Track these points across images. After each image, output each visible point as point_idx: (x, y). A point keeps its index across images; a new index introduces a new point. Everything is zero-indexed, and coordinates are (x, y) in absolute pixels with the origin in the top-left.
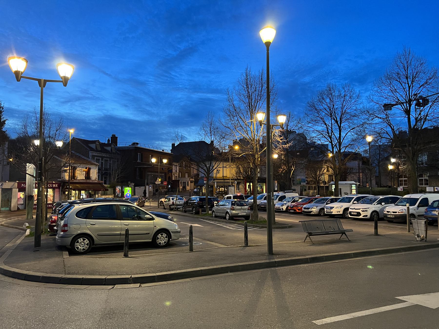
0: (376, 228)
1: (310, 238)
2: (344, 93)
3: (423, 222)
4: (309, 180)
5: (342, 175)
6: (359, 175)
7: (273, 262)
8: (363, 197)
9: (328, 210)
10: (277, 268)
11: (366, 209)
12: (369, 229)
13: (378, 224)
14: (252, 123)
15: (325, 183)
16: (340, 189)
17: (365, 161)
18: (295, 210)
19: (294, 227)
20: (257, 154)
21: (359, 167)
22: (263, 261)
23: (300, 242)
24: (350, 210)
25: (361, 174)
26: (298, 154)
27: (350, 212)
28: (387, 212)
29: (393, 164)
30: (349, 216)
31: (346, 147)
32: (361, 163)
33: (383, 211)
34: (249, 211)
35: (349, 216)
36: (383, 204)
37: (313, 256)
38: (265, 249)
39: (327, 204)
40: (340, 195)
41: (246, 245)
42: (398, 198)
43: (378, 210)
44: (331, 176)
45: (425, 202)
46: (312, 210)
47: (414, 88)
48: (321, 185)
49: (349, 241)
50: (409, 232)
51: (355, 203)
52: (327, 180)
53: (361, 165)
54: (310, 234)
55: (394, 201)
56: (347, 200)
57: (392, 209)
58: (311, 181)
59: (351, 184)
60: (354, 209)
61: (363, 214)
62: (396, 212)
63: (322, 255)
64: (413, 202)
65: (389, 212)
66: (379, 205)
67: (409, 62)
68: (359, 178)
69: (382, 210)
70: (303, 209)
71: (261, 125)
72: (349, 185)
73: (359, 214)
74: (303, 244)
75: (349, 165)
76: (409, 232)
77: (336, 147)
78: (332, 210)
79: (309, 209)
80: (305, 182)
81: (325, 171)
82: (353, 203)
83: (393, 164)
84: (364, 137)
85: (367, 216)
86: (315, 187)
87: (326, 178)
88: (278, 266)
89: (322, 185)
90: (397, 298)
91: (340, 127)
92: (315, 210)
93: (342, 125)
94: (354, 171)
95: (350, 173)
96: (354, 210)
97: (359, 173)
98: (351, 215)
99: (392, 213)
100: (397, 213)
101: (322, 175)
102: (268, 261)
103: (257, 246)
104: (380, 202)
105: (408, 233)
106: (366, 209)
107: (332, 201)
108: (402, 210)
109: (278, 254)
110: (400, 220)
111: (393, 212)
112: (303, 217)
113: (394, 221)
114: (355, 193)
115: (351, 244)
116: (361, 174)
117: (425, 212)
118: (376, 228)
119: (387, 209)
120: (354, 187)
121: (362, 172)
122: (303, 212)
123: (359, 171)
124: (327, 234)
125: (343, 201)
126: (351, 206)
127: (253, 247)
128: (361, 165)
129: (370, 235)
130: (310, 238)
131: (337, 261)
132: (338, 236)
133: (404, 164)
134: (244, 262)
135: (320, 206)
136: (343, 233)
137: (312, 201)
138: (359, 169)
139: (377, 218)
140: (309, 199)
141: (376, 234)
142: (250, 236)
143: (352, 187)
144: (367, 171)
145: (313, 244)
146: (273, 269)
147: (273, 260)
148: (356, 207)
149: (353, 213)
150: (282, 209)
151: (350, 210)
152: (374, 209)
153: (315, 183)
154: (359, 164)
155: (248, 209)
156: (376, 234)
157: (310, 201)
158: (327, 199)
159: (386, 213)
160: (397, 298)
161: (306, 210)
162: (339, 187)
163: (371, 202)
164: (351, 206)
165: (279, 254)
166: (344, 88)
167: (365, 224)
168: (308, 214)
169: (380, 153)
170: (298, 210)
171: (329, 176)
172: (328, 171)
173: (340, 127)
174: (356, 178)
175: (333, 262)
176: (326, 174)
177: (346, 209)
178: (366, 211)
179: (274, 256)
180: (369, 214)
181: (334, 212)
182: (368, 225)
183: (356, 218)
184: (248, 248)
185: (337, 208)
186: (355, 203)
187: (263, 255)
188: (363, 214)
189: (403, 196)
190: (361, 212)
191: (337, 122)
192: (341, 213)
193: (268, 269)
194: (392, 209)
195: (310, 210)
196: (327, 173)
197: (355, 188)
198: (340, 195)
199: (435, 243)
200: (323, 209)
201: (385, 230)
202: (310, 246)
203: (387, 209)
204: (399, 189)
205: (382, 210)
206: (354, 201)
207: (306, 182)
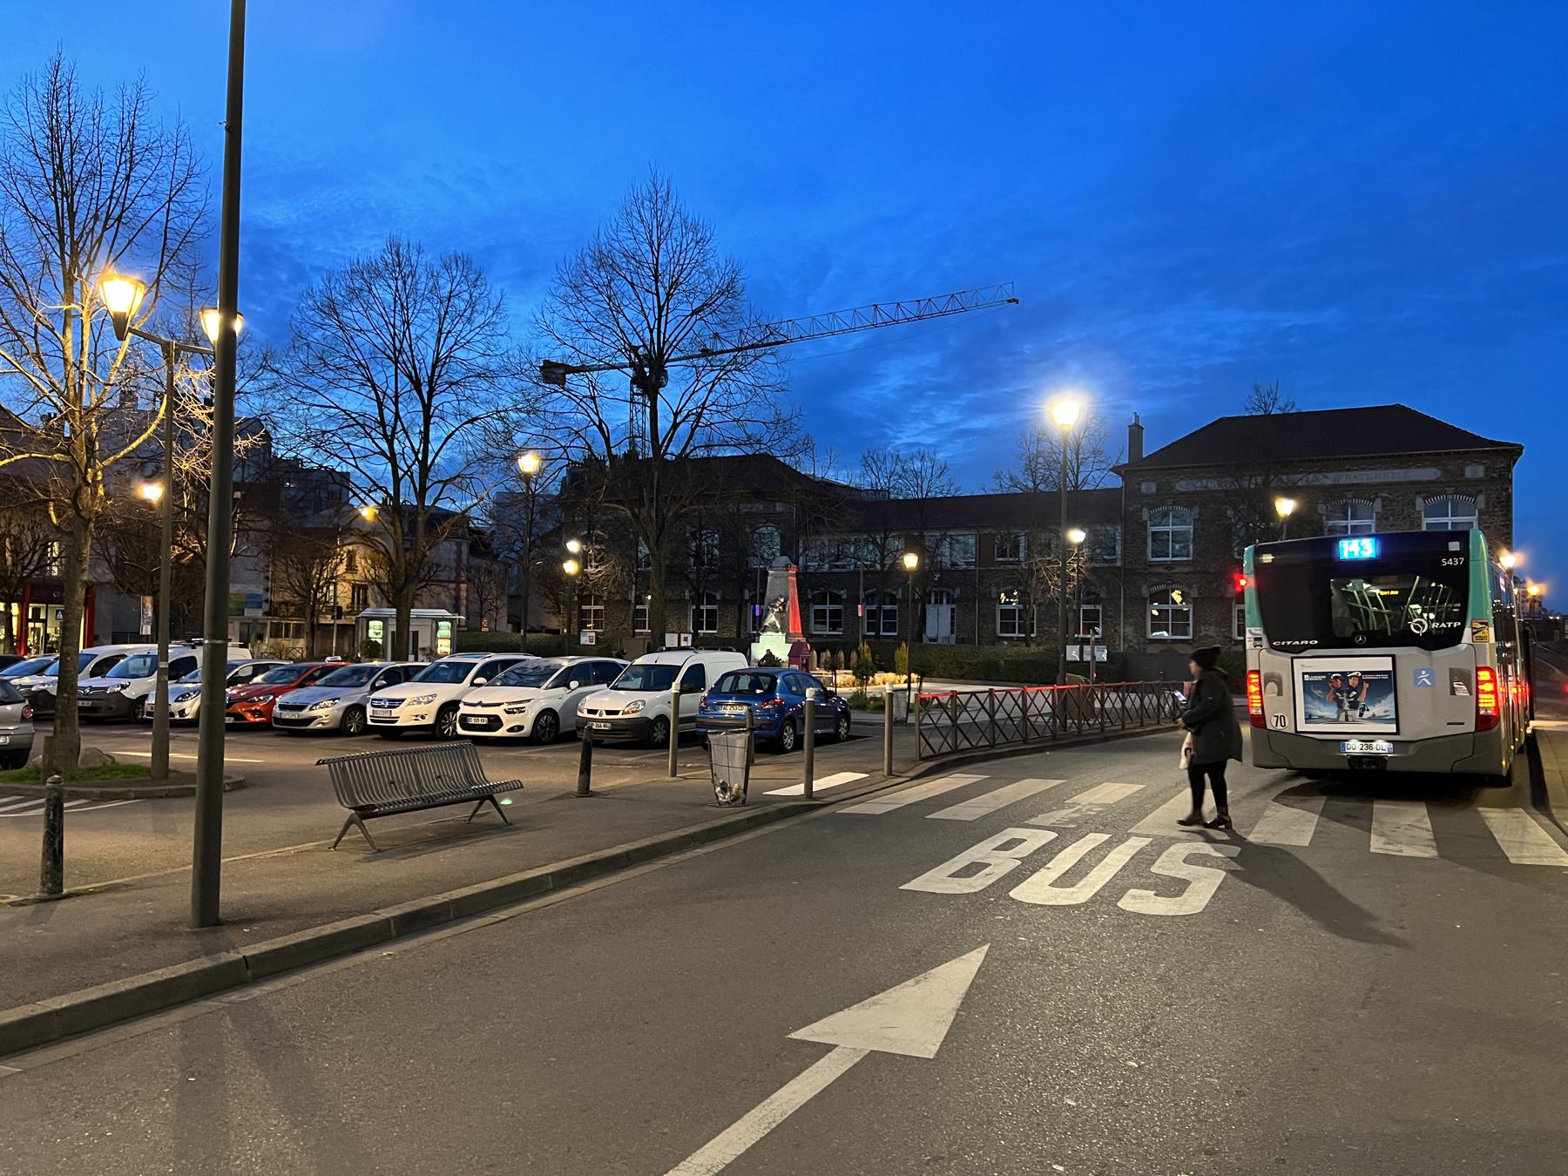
0: (585, 769)
1: (362, 826)
2: (448, 288)
3: (740, 741)
4: (277, 598)
5: (401, 587)
6: (458, 590)
7: (224, 959)
8: (506, 664)
9: (381, 713)
10: (256, 992)
11: (515, 705)
12: (554, 773)
13: (594, 757)
14: (72, 321)
15: (338, 612)
16: (416, 634)
17: (479, 543)
18: (238, 716)
19: (253, 785)
20: (93, 467)
21: (459, 560)
22: (181, 969)
23: (316, 850)
24: (463, 710)
25: (463, 586)
26: (238, 495)
27: (464, 717)
28: (590, 711)
29: (569, 556)
30: (460, 731)
31: (445, 483)
32: (465, 549)
33: (576, 708)
34: (29, 727)
35: (460, 731)
36: (574, 684)
37: (407, 908)
38: (182, 897)
39: (374, 689)
40: (411, 657)
41: (51, 892)
42: (618, 668)
43: (557, 705)
44: (360, 587)
45: (696, 677)
46: (315, 713)
47: (670, 317)
48: (322, 621)
49: (506, 826)
50: (674, 775)
51: (480, 685)
52: (344, 602)
53: (464, 557)
54: (365, 812)
55: (605, 675)
56: (449, 675)
57: (607, 703)
58: (286, 603)
59: (437, 620)
60: (480, 704)
61: (508, 722)
62: (617, 712)
63: (440, 899)
64: (659, 678)
65: (594, 712)
66: (562, 690)
67: (666, 224)
68: (457, 598)
69: (574, 704)
70: (276, 710)
71: (121, 337)
72: (429, 622)
73: (495, 722)
74: (333, 856)
75: (421, 549)
76: (674, 775)
77: (411, 477)
78: (395, 712)
79: (301, 708)
80: (260, 607)
81: (342, 568)
82: (472, 684)
83: (574, 557)
84: (512, 458)
85: (521, 728)
86: (298, 628)
87: (343, 594)
88: (257, 979)
89: (327, 620)
90: (794, 1036)
91: (427, 408)
92: (326, 712)
93: (435, 403)
94: (443, 575)
95: (429, 581)
96: (479, 710)
97: (458, 582)
98: (465, 726)
99: (605, 716)
100: (620, 716)
101: (328, 583)
102: (205, 963)
103: (108, 889)
104: (563, 681)
105: (668, 778)
106: (515, 705)
107: (393, 677)
108: (635, 703)
109: (242, 920)
110: (639, 737)
111: (608, 713)
112: (278, 741)
113: (606, 741)
114: (448, 650)
115: (522, 836)
116: (463, 586)
117: (702, 709)
118: (585, 769)
119: (589, 702)
120: (445, 629)
121: (469, 580)
122: (278, 720)
123: (458, 575)
124: (431, 804)
125: (433, 676)
126: (465, 693)
127: (92, 899)
128: (464, 557)
129: (562, 797)
130: (362, 826)
131: (503, 915)
132: (459, 813)
133: (601, 561)
134: (77, 987)
135: (346, 698)
136: (487, 796)
137: (312, 679)
138: (458, 568)
139: (551, 731)
140: (299, 671)
141: (585, 790)
142: (75, 844)
143: (437, 628)
144: (491, 573)
145: (377, 851)
146: (235, 997)
147: (234, 956)
148: (484, 699)
149: (472, 721)
150: (182, 712)
151: (463, 710)
152: (544, 704)
153: (300, 612)
154: (459, 553)
155: (23, 719)
156: (585, 790)
157: (306, 680)
158: (374, 670)
159: (585, 715)
160: (794, 1036)
161: (287, 715)
162: (412, 629)
163: (534, 679)
164: (465, 693)
165: (248, 921)
166: (447, 268)
167: (516, 758)
168: (299, 731)
169: (536, 518)
170: (254, 713)
171: (356, 587)
172: (351, 568)
173: (427, 408)
174: (448, 601)
175: (489, 919)
176: (347, 575)
177: (451, 706)
178: (521, 710)
179: (231, 934)
180: (527, 720)
181: (405, 717)
182: (530, 759)
183: (488, 738)
184: (62, 905)
185: (415, 704)
186: (480, 685)
187: (162, 932)
188: (508, 722)
189: (632, 660)
190: (504, 717)
191: (417, 385)
192: (430, 720)
193: (211, 1004)
194: (607, 703)
195: (306, 713)
196: (349, 576)
197: (447, 633)
198: (411, 657)
199: (770, 809)
200: (360, 708)
201: (616, 775)
202: (368, 860)
203: (589, 702)
204: (584, 640)
205: (574, 704)
206: (476, 676)
207: (266, 607)
